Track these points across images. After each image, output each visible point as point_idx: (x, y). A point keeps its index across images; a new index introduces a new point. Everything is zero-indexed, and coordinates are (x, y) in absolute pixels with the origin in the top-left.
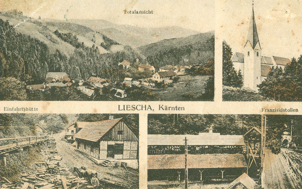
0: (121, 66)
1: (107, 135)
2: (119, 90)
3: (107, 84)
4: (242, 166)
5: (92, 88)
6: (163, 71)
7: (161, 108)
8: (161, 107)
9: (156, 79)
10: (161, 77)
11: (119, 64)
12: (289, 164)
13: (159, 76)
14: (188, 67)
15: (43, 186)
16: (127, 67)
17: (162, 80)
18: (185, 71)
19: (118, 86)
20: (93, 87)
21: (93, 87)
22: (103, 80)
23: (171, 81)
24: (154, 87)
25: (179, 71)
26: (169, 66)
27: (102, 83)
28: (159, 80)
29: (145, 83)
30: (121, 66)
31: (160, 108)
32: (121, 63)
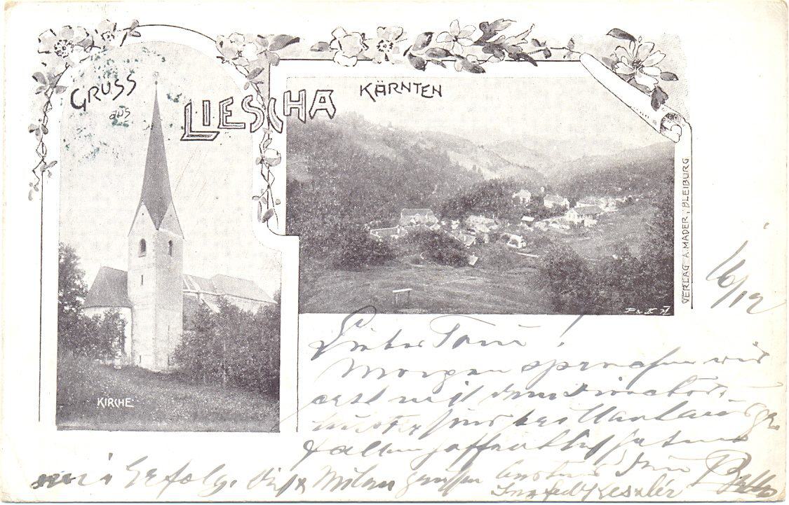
0: (517, 198)
1: (271, 328)
2: (513, 237)
3: (495, 227)
4: (277, 52)
5: (473, 233)
6: (583, 205)
7: (364, 91)
8: (365, 89)
9: (571, 219)
10: (578, 216)
11: (514, 196)
12: (150, 122)
13: (576, 214)
14: (620, 200)
15: (459, 473)
16: (527, 201)
17: (580, 220)
18: (616, 206)
19: (513, 230)
20: (473, 231)
21: (473, 231)
22: (489, 220)
23: (595, 222)
24: (568, 231)
25: (607, 206)
26: (592, 198)
27: (488, 225)
28: (577, 221)
29: (554, 225)
30: (517, 198)
31: (361, 91)
32: (516, 195)
